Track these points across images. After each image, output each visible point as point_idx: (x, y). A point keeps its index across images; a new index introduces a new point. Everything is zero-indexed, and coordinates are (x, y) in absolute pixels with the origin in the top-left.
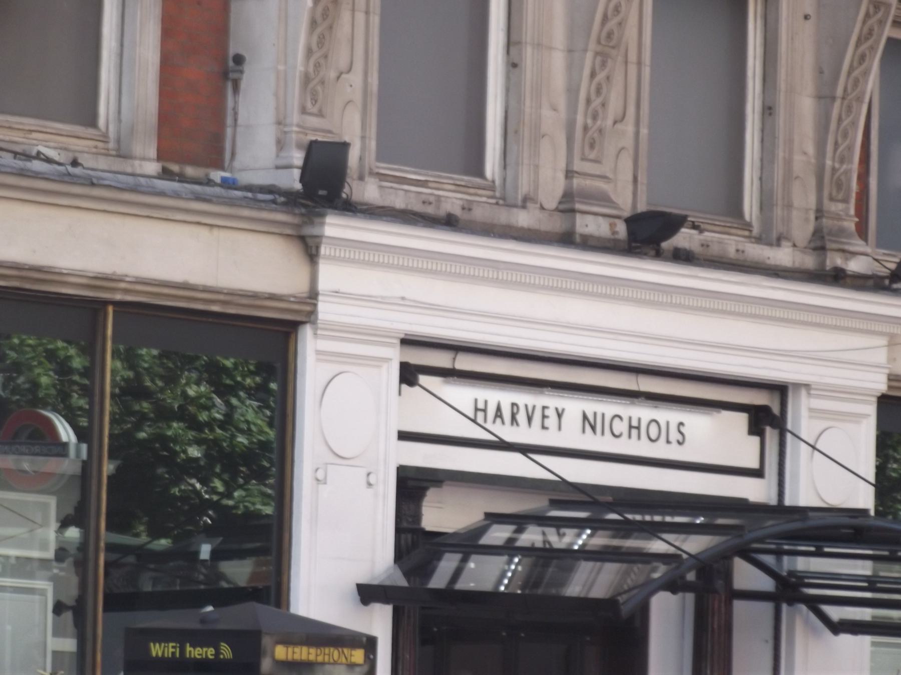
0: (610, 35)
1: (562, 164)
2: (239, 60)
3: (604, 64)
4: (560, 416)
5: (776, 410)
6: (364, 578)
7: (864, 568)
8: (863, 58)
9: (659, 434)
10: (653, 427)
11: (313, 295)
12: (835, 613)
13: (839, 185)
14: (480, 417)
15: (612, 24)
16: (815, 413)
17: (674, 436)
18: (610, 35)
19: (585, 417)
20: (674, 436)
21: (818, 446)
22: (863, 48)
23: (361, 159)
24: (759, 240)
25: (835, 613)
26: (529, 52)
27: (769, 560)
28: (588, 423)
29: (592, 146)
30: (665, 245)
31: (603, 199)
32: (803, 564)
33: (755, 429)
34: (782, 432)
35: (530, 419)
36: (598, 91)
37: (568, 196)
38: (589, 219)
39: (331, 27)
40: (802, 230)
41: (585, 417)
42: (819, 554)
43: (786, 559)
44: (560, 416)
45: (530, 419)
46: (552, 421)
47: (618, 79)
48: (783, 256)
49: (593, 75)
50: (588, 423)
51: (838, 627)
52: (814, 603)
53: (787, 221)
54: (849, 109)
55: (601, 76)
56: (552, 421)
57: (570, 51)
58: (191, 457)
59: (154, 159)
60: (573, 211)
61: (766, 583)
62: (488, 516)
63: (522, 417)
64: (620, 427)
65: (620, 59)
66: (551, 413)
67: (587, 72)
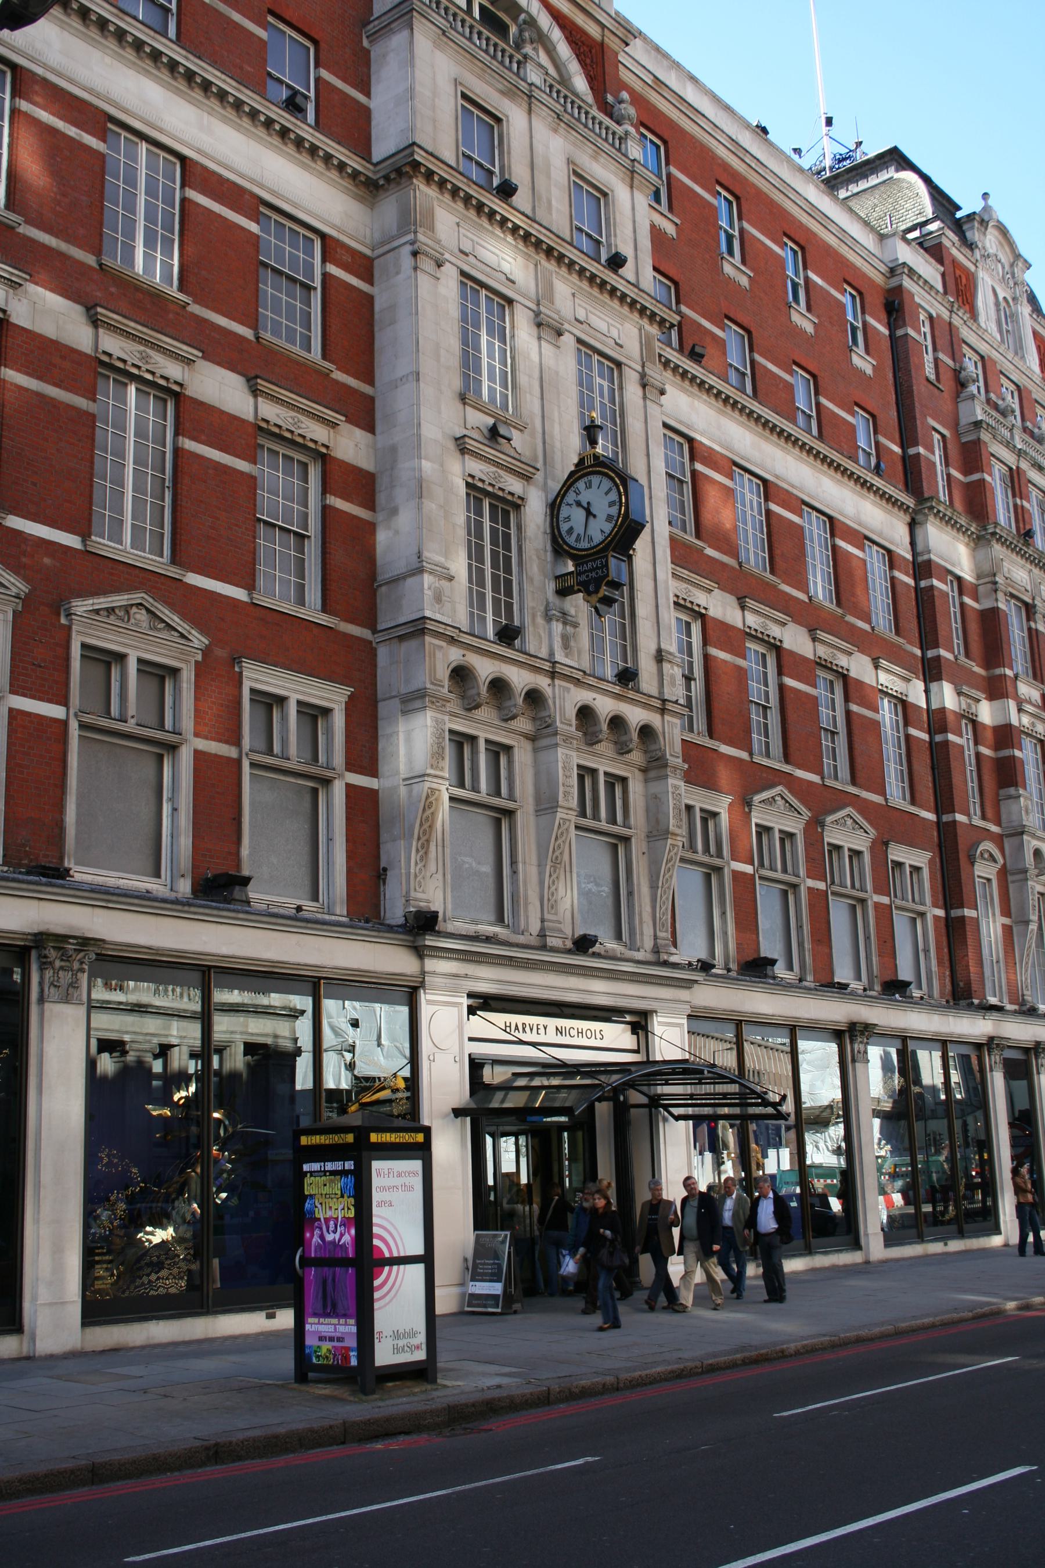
0: (557, 858)
1: (539, 915)
2: (385, 870)
3: (555, 871)
4: (545, 1028)
5: (643, 1023)
6: (456, 1105)
7: (689, 1089)
8: (669, 870)
9: (593, 1034)
10: (589, 1033)
11: (423, 973)
12: (676, 1111)
13: (663, 925)
14: (508, 1030)
15: (557, 853)
16: (660, 1023)
17: (599, 1036)
18: (557, 858)
19: (557, 1029)
20: (599, 1036)
21: (419, 1250)
22: (670, 865)
23: (306, 480)
24: (630, 949)
25: (676, 1111)
26: (520, 866)
27: (645, 1089)
28: (559, 1031)
29: (552, 907)
30: (591, 950)
31: (560, 931)
32: (660, 1090)
33: (634, 1031)
34: (646, 1032)
35: (531, 1030)
36: (554, 882)
37: (542, 929)
38: (553, 939)
39: (426, 853)
40: (649, 944)
41: (557, 1029)
42: (667, 1084)
43: (652, 1087)
44: (545, 1028)
45: (531, 1030)
46: (542, 1031)
47: (562, 877)
48: (640, 956)
49: (550, 876)
50: (559, 1031)
51: (678, 1118)
52: (666, 1107)
53: (642, 940)
54: (665, 893)
55: (554, 876)
56: (542, 1031)
57: (539, 866)
58: (667, 1260)
59: (175, 682)
60: (545, 936)
61: (644, 1100)
62: (514, 1074)
63: (528, 1029)
64: (574, 1032)
65: (562, 870)
66: (541, 1027)
67: (547, 874)
